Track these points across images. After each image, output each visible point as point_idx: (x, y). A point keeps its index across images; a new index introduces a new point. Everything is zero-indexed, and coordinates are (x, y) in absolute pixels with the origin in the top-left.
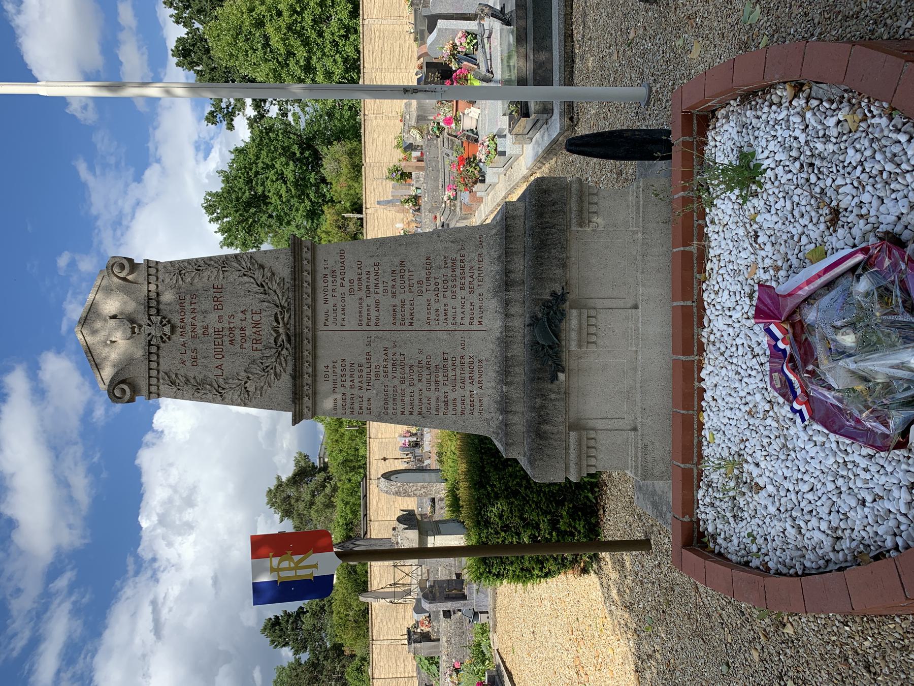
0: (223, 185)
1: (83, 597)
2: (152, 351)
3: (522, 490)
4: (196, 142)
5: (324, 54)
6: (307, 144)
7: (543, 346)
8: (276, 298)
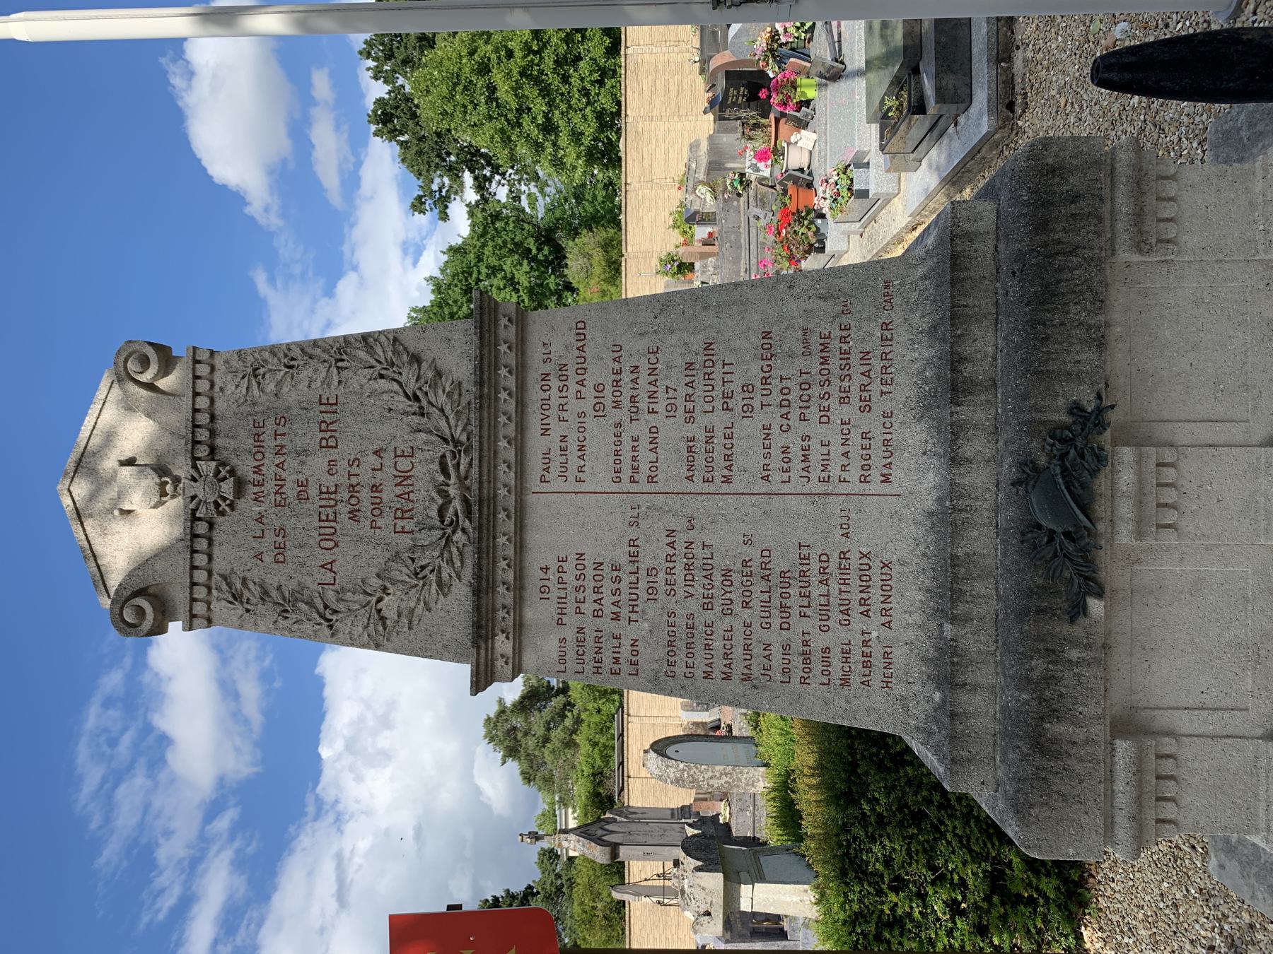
0: (432, 297)
1: (248, 845)
2: (198, 530)
3: (932, 812)
4: (404, 243)
5: (570, 107)
6: (547, 236)
7: (1052, 532)
8: (443, 423)
